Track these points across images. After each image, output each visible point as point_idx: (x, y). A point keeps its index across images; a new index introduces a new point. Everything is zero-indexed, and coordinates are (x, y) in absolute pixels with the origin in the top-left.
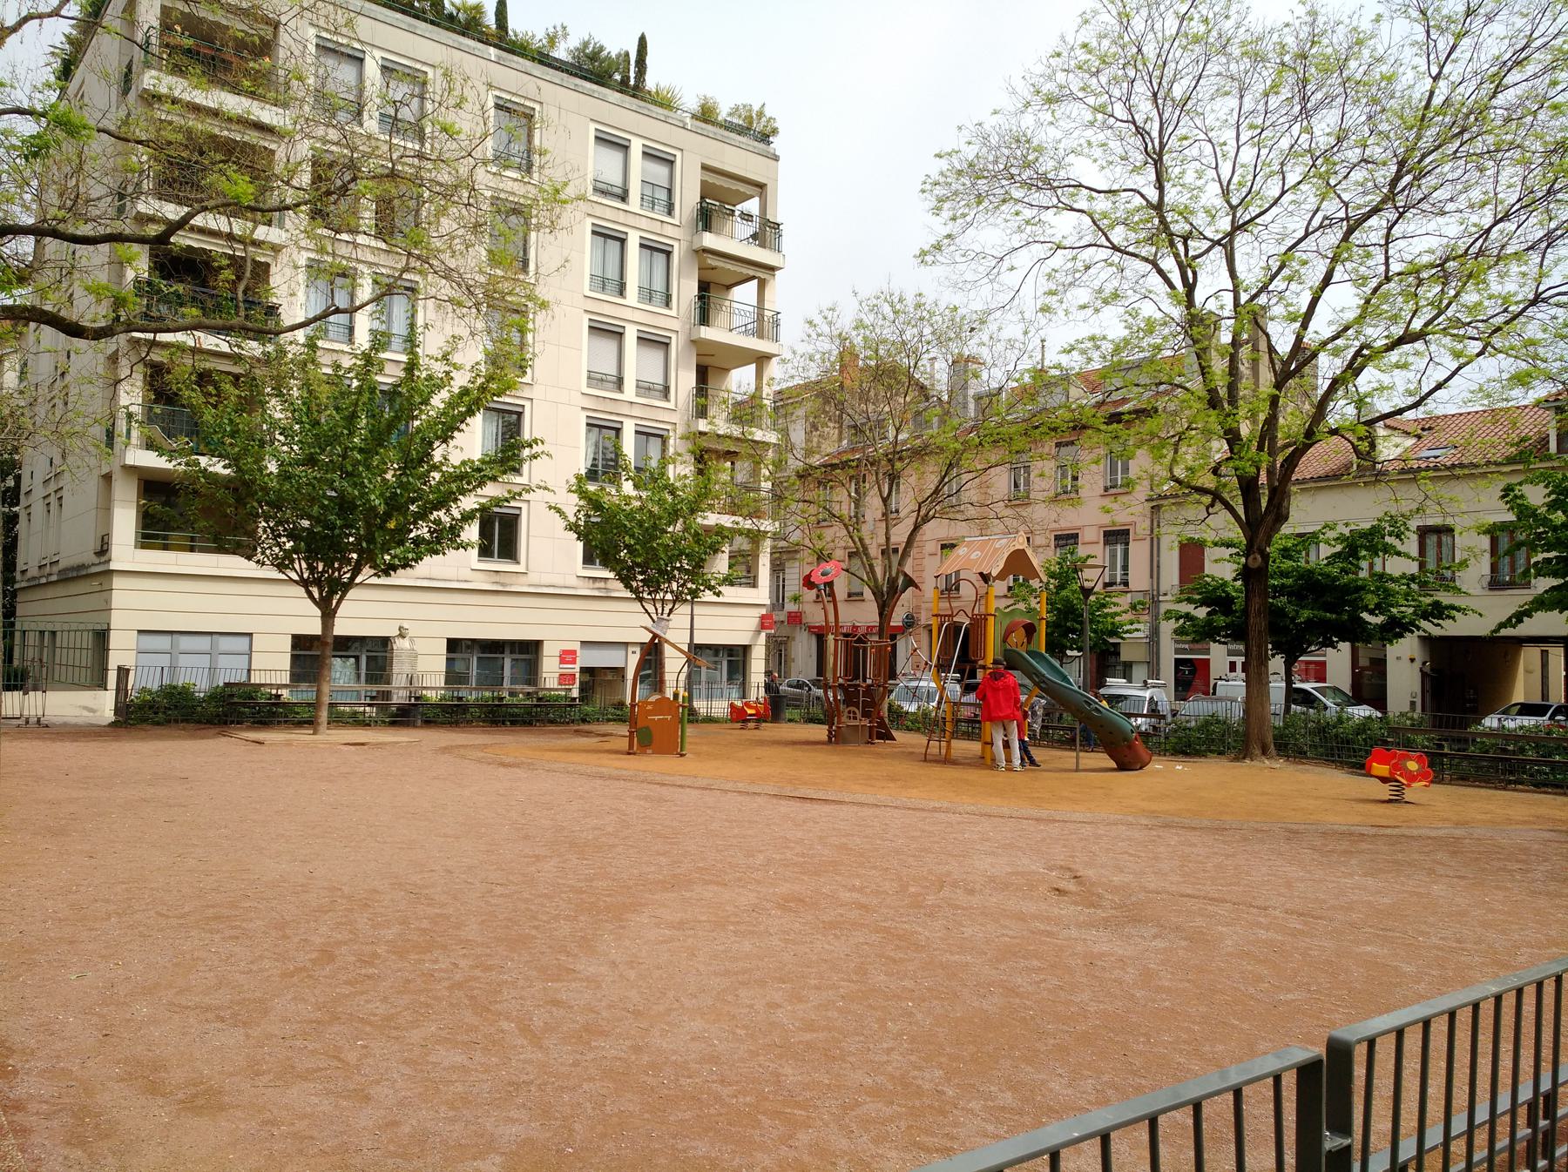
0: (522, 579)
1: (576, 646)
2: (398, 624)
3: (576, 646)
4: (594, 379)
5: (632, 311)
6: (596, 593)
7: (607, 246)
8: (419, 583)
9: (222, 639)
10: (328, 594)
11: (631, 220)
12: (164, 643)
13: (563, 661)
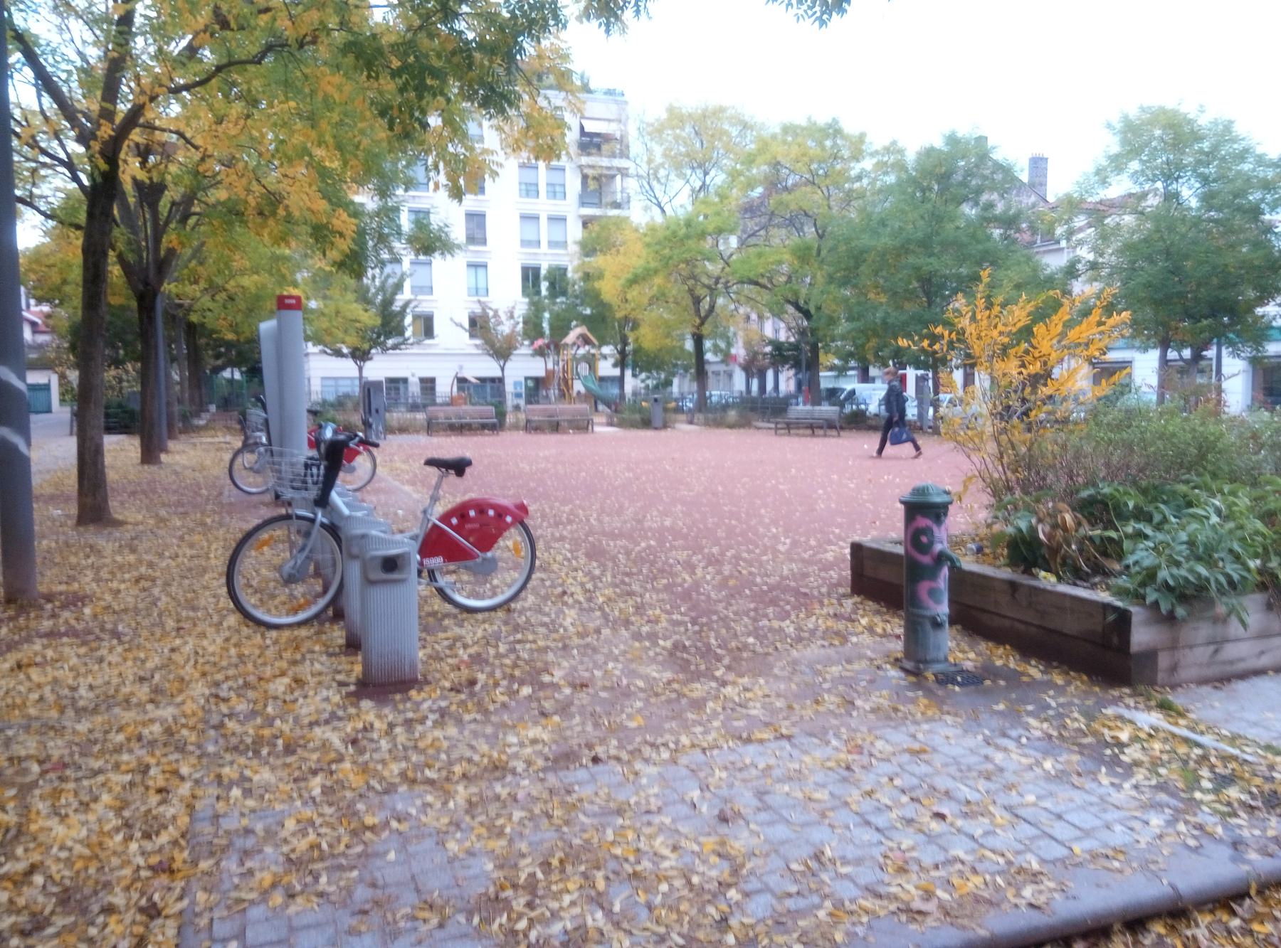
12: (332, 383)
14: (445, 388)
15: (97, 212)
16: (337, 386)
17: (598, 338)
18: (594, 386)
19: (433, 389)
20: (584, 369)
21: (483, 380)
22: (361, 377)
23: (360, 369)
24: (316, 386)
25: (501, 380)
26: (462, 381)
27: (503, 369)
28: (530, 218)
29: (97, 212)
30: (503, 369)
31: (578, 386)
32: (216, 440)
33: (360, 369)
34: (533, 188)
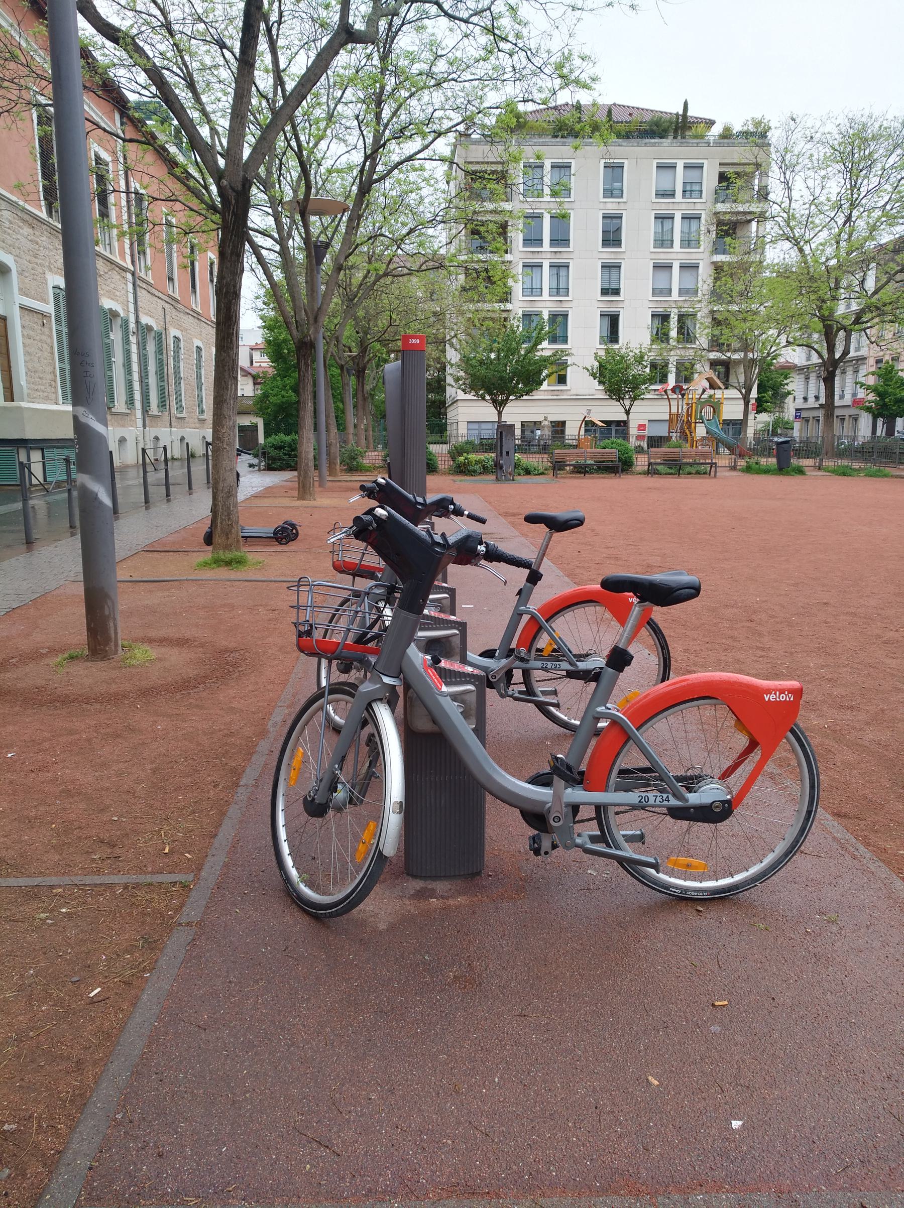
0: (568, 392)
1: (646, 423)
2: (543, 416)
3: (646, 423)
4: (655, 292)
5: (677, 254)
6: (656, 397)
7: (692, 224)
8: (572, 397)
9: (482, 424)
10: (499, 405)
11: (676, 207)
12: (476, 426)
13: (639, 429)
14: (573, 430)
15: (228, 251)
16: (479, 430)
17: (724, 384)
18: (717, 430)
19: (563, 432)
20: (708, 412)
21: (608, 423)
22: (499, 421)
23: (500, 414)
24: (463, 429)
25: (625, 423)
26: (589, 425)
27: (628, 412)
28: (662, 267)
29: (228, 251)
30: (628, 412)
31: (701, 431)
32: (220, 510)
33: (500, 414)
34: (697, 187)
